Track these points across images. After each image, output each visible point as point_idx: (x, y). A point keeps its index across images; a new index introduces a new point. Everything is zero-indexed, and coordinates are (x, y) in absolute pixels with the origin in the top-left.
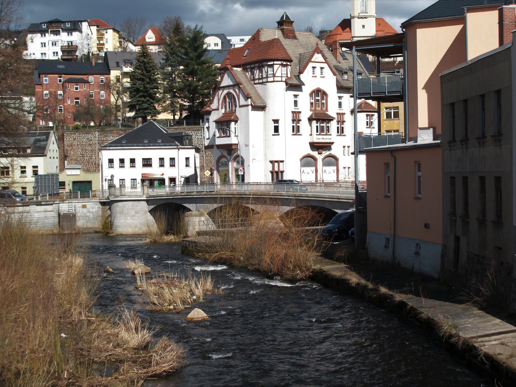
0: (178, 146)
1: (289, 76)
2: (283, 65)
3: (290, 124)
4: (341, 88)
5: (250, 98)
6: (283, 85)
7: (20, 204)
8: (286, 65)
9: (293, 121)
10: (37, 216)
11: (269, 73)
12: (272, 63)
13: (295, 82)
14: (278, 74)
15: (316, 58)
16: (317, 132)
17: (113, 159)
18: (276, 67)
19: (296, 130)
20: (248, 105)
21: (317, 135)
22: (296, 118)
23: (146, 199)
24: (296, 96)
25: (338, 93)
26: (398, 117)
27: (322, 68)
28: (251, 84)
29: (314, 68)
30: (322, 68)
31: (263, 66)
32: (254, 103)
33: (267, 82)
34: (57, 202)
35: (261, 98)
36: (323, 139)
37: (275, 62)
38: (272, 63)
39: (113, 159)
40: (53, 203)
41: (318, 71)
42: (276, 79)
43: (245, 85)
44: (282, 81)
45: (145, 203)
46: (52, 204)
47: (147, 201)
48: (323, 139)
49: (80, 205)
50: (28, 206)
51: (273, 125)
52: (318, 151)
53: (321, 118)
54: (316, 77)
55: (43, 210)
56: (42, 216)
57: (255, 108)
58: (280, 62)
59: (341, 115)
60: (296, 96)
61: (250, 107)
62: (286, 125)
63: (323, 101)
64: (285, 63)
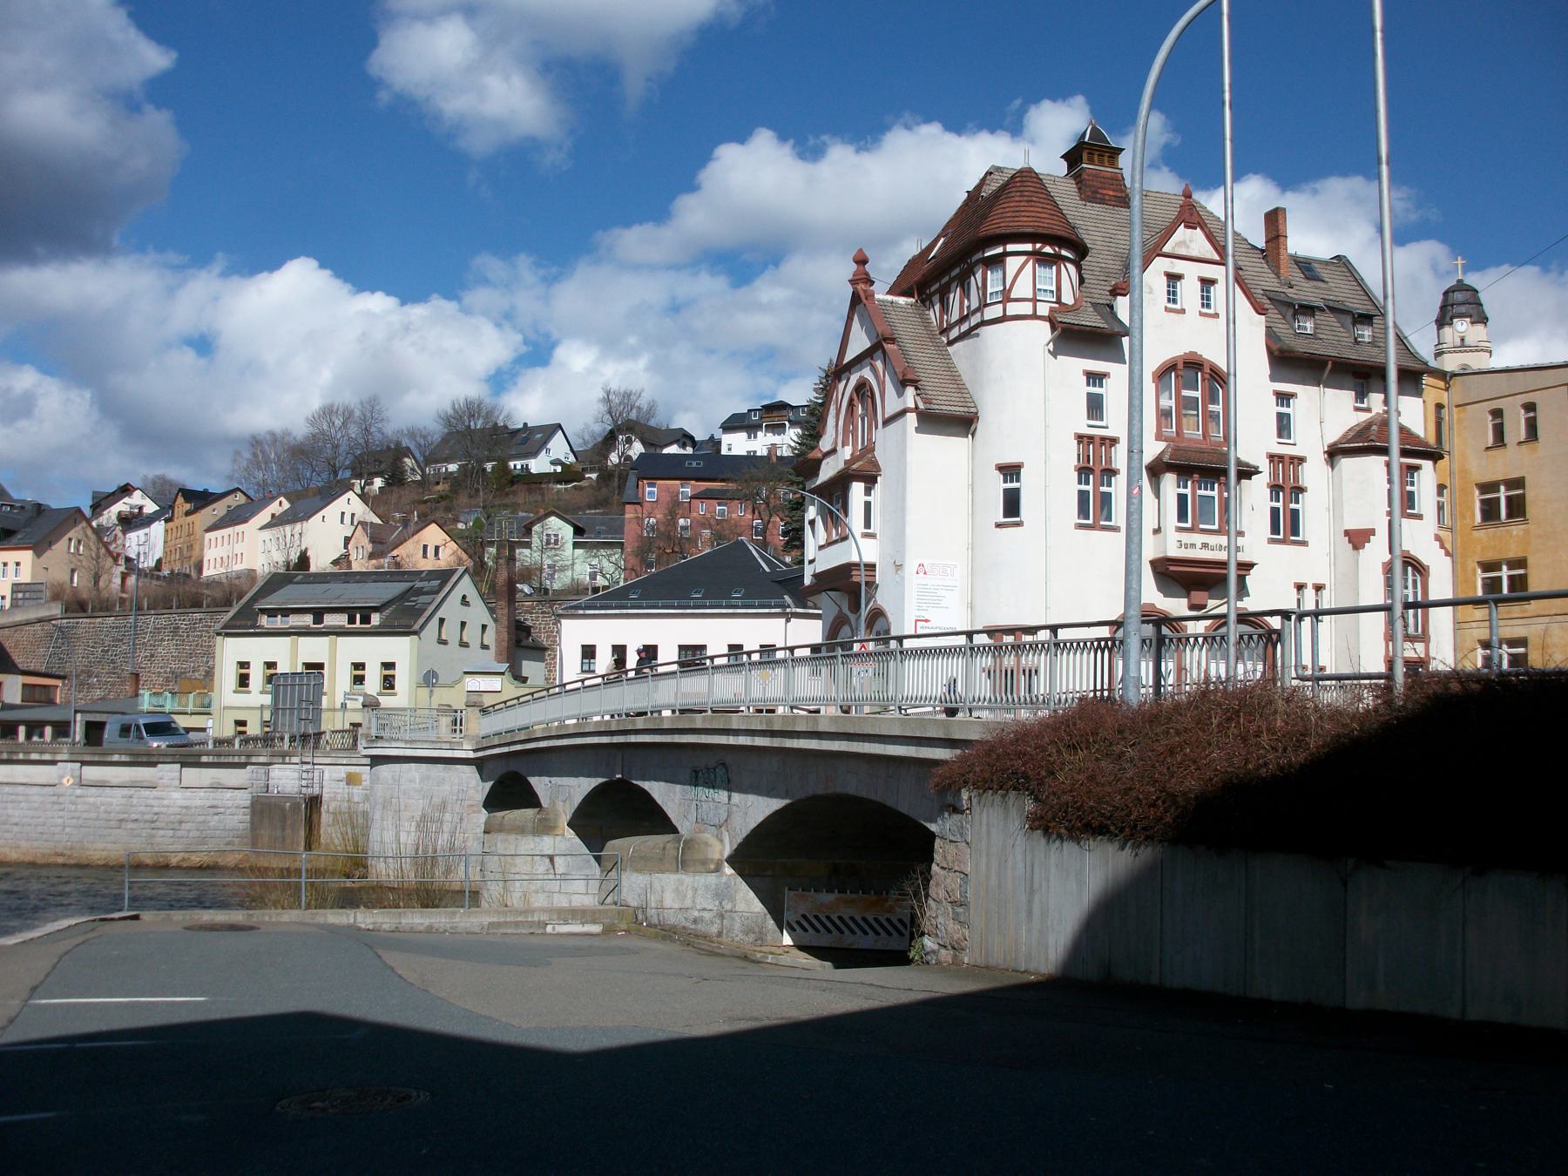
0: (784, 606)
1: (1068, 298)
2: (1043, 260)
3: (1070, 486)
4: (1290, 362)
5: (914, 382)
6: (1042, 332)
7: (124, 758)
8: (1055, 260)
9: (1084, 472)
10: (181, 802)
11: (989, 290)
12: (1000, 250)
13: (1090, 319)
14: (1023, 288)
15: (1182, 243)
16: (1182, 515)
17: (594, 647)
18: (1013, 264)
19: (1093, 510)
20: (903, 413)
21: (1180, 530)
22: (1094, 461)
23: (471, 755)
24: (1095, 378)
25: (1273, 378)
26: (1524, 515)
27: (1207, 283)
28: (938, 346)
29: (1173, 278)
30: (1207, 283)
31: (970, 272)
32: (926, 401)
33: (984, 323)
34: (262, 759)
35: (960, 387)
36: (1205, 546)
37: (1011, 247)
38: (1000, 250)
39: (594, 647)
40: (243, 759)
41: (1189, 291)
42: (1013, 309)
43: (909, 345)
44: (1034, 316)
45: (470, 772)
46: (243, 765)
47: (479, 764)
48: (1205, 546)
49: (342, 772)
50: (154, 764)
51: (999, 485)
52: (1188, 596)
53: (1202, 468)
54: (1183, 311)
55: (206, 783)
56: (199, 803)
57: (933, 421)
58: (1028, 247)
59: (1286, 464)
60: (1095, 378)
61: (911, 419)
62: (1052, 487)
63: (1212, 407)
64: (1048, 249)
